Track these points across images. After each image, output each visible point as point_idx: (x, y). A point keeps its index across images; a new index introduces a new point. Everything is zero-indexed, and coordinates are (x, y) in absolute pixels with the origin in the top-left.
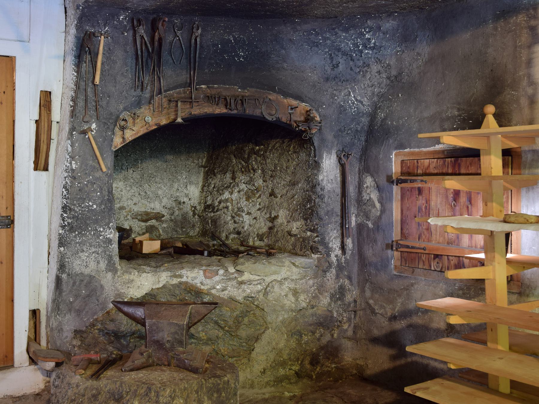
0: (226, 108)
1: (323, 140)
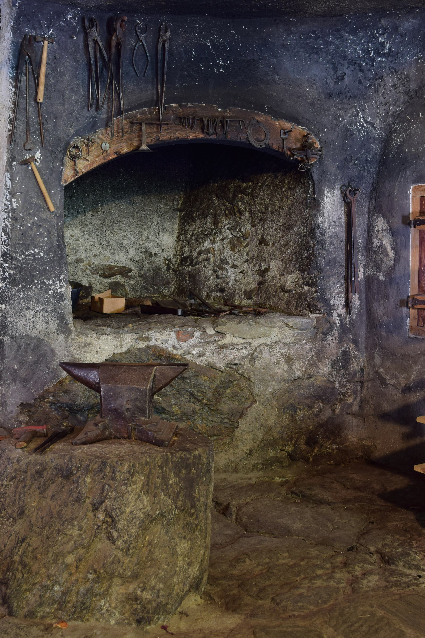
0: (203, 132)
1: (324, 173)
